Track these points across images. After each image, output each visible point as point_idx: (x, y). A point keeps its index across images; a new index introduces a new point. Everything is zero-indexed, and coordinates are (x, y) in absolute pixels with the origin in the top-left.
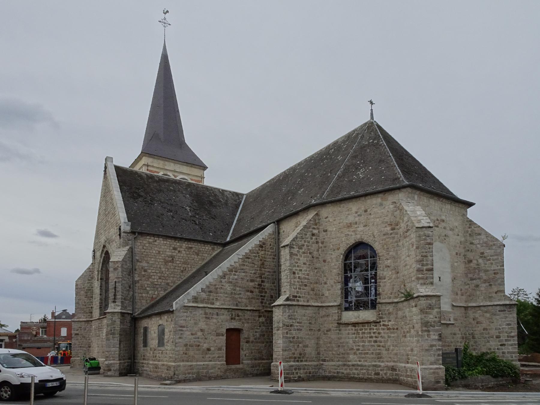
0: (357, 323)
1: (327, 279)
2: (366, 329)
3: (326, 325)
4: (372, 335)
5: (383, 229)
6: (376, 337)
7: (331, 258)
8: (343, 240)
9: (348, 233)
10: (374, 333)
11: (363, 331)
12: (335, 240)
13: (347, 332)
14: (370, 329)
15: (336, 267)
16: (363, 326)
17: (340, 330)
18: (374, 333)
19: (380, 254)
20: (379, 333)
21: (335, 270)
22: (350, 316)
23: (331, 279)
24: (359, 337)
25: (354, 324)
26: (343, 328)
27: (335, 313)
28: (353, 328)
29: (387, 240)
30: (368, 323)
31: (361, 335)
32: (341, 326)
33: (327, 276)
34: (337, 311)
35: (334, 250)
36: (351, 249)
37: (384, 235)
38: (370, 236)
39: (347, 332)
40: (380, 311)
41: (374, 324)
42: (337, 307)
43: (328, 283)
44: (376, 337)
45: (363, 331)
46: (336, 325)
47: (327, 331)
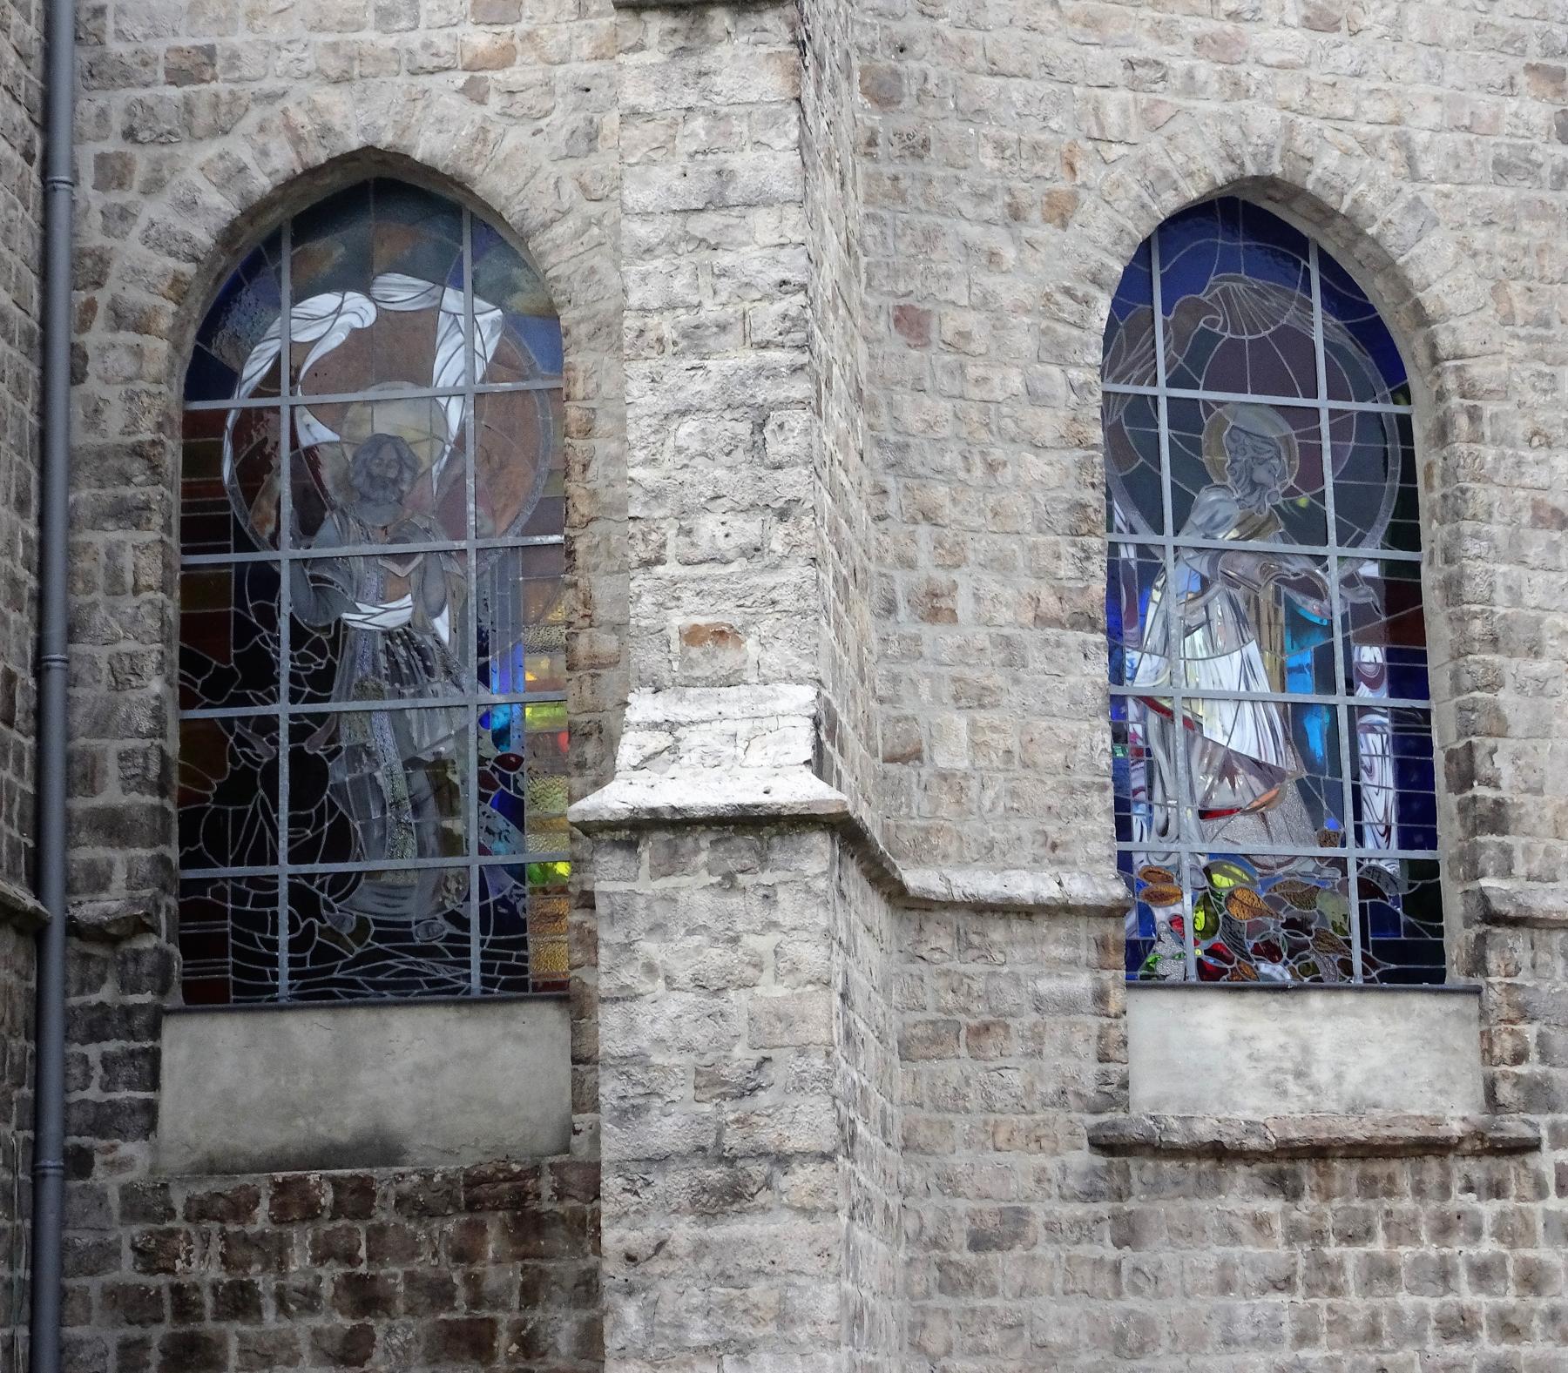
0: (1318, 1152)
1: (953, 558)
2: (1401, 1230)
3: (960, 1161)
4: (1467, 1296)
5: (1485, 103)
6: (1508, 1328)
7: (985, 302)
8: (1112, 116)
9: (1150, 48)
10: (1483, 1273)
11: (1379, 1246)
12: (1017, 90)
13: (1210, 1255)
14: (1444, 1228)
15: (1048, 423)
16: (1368, 1186)
17: (1128, 1233)
18: (1483, 1273)
19: (1478, 370)
20: (1533, 1279)
21: (1036, 466)
22: (1227, 1056)
23: (1001, 565)
24: (1339, 1323)
25: (1291, 1161)
26: (1169, 1209)
27: (1069, 1006)
28: (1272, 1206)
29: (1534, 231)
30: (1432, 1147)
31: (1355, 1303)
32: (1141, 1170)
33: (949, 512)
34: (1083, 983)
35: (1016, 214)
36: (272, 243)
37: (1503, 169)
38: (1369, 146)
39: (1210, 1255)
40: (1525, 1013)
41: (1477, 1169)
42: (1088, 930)
43: (963, 604)
44: (1508, 1328)
45: (1379, 1246)
46: (1082, 1158)
47: (979, 1242)
